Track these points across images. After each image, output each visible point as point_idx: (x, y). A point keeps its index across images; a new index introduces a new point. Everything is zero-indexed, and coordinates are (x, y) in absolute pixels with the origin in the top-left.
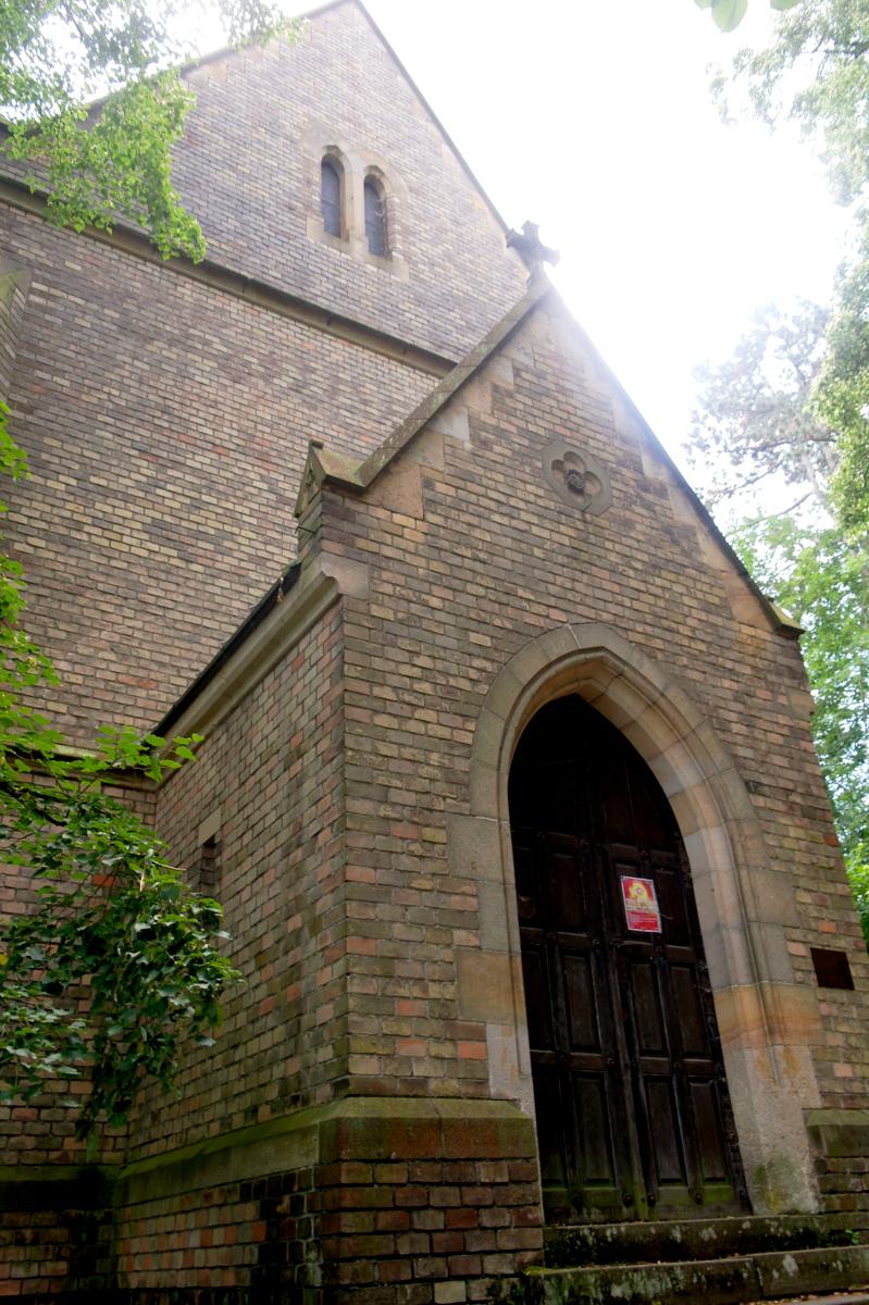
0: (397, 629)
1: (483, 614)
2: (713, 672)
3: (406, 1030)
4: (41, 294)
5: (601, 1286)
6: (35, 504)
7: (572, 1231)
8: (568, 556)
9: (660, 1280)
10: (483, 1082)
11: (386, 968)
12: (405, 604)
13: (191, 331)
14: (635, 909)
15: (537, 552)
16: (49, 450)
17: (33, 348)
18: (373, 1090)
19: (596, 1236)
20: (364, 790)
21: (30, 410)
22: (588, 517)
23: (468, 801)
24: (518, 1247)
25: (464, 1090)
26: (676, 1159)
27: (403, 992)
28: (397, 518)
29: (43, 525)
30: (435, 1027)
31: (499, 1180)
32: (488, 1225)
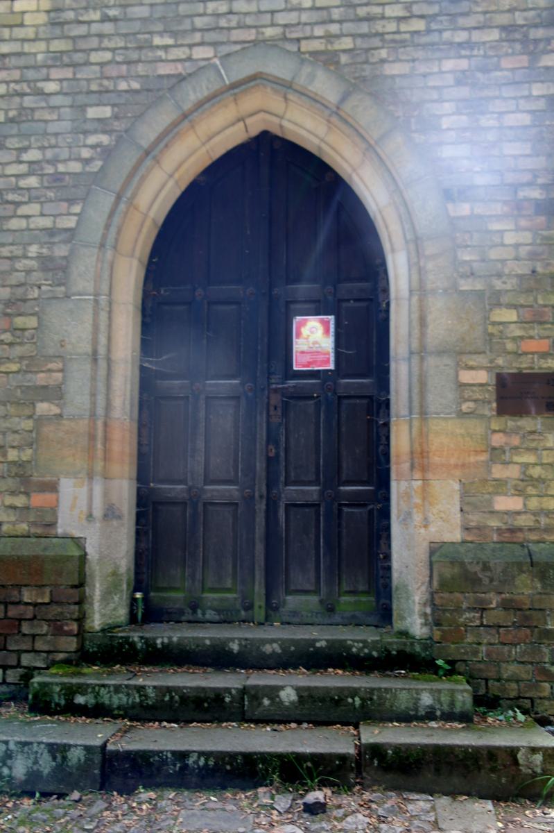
1: (106, 83)
5: (65, 695)
7: (122, 637)
9: (128, 695)
10: (53, 525)
14: (305, 348)
19: (146, 643)
23: (63, 284)
24: (52, 649)
30: (11, 483)
31: (40, 601)
32: (26, 632)
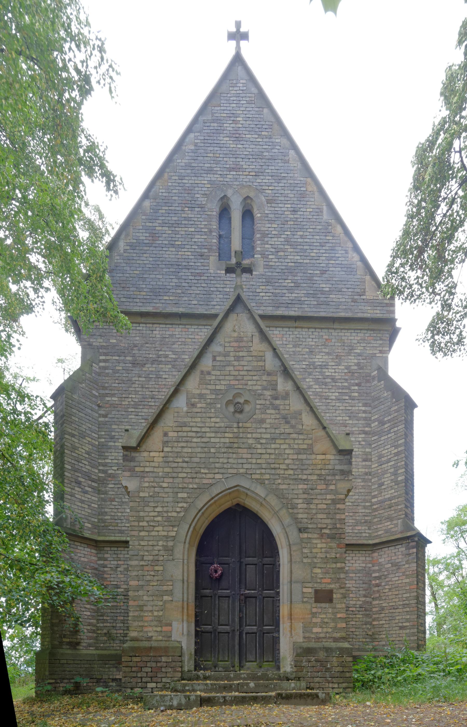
0: (149, 499)
1: (185, 485)
2: (294, 483)
3: (146, 624)
4: (105, 361)
6: (113, 454)
8: (227, 448)
11: (141, 608)
12: (153, 489)
13: (161, 353)
15: (213, 450)
16: (114, 430)
17: (104, 388)
18: (134, 639)
20: (135, 557)
21: (105, 416)
22: (241, 425)
25: (164, 639)
26: (254, 656)
27: (146, 615)
28: (152, 454)
29: (116, 461)
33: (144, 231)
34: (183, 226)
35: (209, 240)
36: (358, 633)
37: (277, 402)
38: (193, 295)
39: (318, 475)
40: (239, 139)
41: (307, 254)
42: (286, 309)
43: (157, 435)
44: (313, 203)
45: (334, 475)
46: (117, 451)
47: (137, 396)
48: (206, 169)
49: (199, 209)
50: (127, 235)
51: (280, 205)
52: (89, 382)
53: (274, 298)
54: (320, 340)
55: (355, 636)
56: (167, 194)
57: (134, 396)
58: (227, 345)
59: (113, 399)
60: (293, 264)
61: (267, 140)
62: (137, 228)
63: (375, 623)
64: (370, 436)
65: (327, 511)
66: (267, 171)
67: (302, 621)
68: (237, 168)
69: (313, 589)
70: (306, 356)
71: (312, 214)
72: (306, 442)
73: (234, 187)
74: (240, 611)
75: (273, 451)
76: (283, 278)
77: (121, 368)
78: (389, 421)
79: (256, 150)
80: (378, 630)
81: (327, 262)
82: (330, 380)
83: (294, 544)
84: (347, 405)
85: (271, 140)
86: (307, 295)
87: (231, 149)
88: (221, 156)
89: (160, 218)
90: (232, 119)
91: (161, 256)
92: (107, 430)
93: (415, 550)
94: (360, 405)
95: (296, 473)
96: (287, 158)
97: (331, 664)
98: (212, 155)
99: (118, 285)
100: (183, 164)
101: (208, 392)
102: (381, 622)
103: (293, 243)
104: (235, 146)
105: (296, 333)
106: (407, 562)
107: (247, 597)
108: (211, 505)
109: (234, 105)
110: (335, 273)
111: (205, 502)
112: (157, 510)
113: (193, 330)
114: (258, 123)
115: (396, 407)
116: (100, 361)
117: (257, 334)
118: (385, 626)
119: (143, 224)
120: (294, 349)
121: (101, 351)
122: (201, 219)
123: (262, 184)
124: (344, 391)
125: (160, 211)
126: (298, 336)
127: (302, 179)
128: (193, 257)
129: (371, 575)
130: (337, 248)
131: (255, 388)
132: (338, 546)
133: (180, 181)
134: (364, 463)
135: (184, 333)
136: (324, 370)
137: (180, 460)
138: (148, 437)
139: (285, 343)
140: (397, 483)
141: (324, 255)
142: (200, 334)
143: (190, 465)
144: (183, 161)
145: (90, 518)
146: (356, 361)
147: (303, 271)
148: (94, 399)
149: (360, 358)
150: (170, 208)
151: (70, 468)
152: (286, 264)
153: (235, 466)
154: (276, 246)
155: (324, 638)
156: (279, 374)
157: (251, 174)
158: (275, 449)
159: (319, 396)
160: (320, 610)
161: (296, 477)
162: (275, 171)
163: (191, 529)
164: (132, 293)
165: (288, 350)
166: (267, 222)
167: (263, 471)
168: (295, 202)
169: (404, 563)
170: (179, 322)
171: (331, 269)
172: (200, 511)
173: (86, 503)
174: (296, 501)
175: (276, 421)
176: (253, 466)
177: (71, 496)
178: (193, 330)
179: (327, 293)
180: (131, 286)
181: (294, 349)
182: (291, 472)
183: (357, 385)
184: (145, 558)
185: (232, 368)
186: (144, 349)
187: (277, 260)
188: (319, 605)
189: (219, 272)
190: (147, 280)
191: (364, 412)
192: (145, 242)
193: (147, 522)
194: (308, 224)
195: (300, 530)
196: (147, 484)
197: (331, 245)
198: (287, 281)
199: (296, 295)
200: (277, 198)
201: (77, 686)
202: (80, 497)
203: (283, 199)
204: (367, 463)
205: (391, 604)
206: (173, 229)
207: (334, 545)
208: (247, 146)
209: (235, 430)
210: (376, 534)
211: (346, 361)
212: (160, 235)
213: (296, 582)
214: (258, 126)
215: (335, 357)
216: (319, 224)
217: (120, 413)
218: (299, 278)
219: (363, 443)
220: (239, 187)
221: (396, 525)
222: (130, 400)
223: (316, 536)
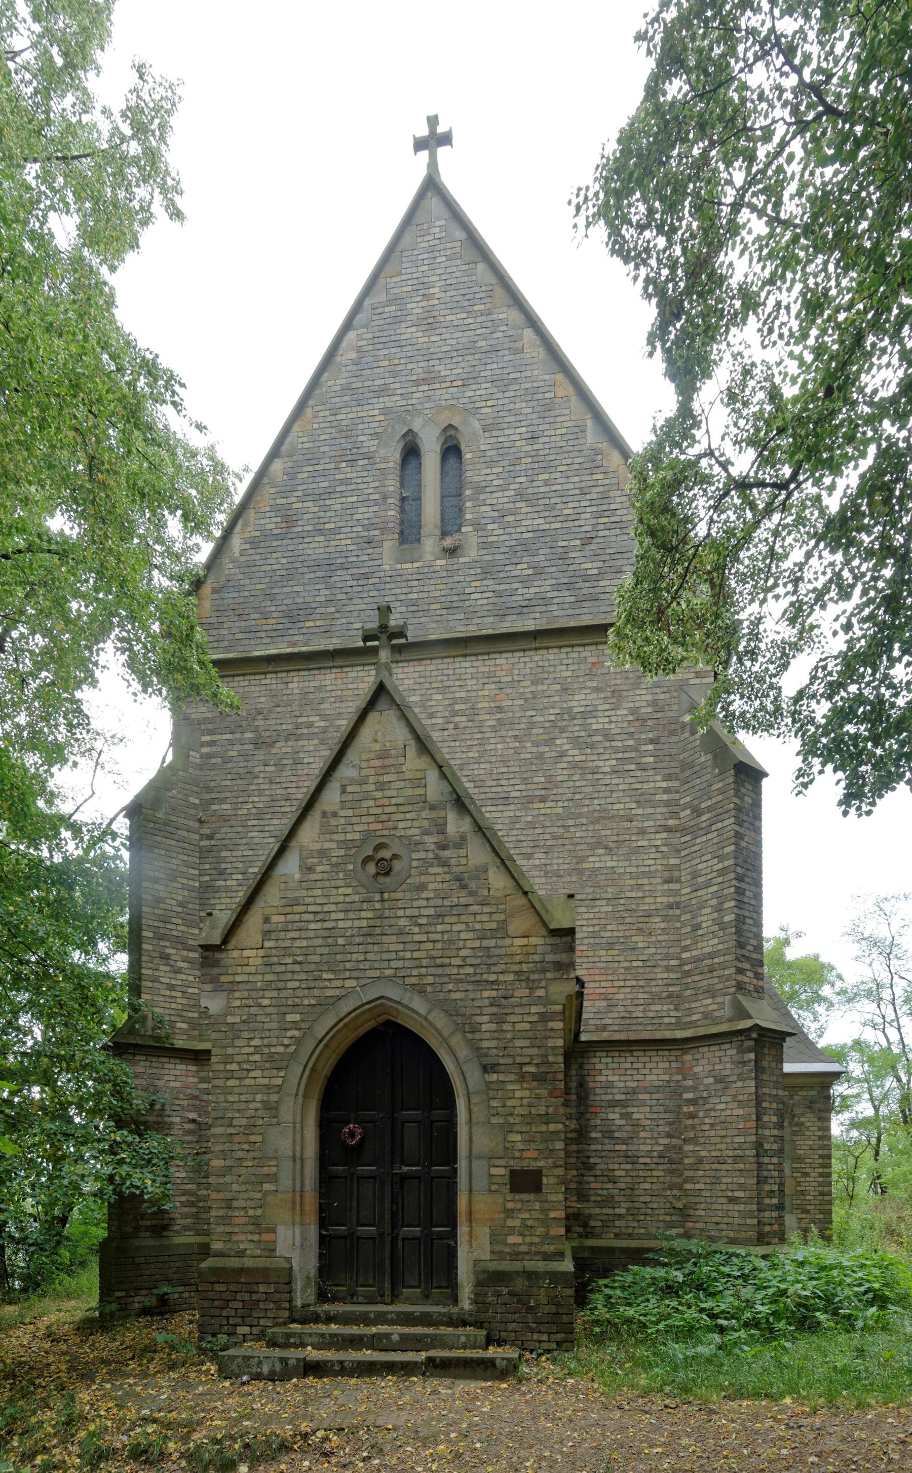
0: (241, 1027)
3: (236, 1230)
4: (210, 744)
6: (222, 900)
10: (274, 1250)
11: (229, 1204)
13: (301, 720)
15: (341, 941)
17: (209, 790)
18: (221, 1254)
20: (220, 1122)
21: (210, 837)
27: (236, 1214)
28: (246, 953)
33: (273, 514)
34: (338, 495)
35: (383, 513)
36: (655, 1206)
37: (446, 853)
38: (355, 614)
39: (516, 973)
40: (434, 326)
41: (556, 513)
42: (519, 617)
43: (254, 921)
44: (567, 418)
45: (544, 971)
46: (229, 894)
47: (262, 799)
48: (377, 388)
49: (366, 461)
50: (246, 525)
51: (507, 432)
52: (183, 785)
53: (495, 600)
54: (582, 667)
55: (649, 1211)
56: (311, 445)
57: (256, 799)
58: (364, 765)
59: (224, 806)
60: (531, 535)
61: (484, 318)
62: (262, 510)
63: (688, 1186)
64: (678, 835)
65: (531, 1034)
66: (483, 374)
67: (489, 1224)
68: (431, 378)
69: (508, 1169)
70: (556, 699)
71: (566, 437)
72: (495, 917)
73: (425, 412)
74: (393, 1201)
75: (438, 937)
76: (513, 561)
77: (235, 753)
78: (709, 809)
79: (464, 340)
80: (692, 1199)
81: (594, 521)
82: (600, 738)
83: (475, 1093)
84: (633, 780)
85: (490, 318)
86: (558, 587)
87: (419, 347)
88: (402, 361)
89: (300, 487)
90: (421, 292)
91: (301, 552)
92: (213, 860)
93: (752, 1056)
94: (658, 778)
95: (478, 971)
96: (519, 345)
97: (536, 1300)
98: (386, 363)
99: (231, 613)
100: (338, 388)
101: (334, 845)
102: (698, 1186)
103: (531, 497)
104: (426, 339)
105: (537, 658)
106: (741, 1077)
107: (404, 1178)
108: (338, 1032)
109: (426, 268)
110: (608, 539)
111: (328, 1028)
112: (253, 1043)
113: (355, 674)
114: (466, 291)
115: (720, 785)
116: (203, 745)
117: (412, 743)
118: (704, 1194)
119: (272, 502)
120: (533, 689)
121: (203, 727)
122: (368, 479)
123: (474, 399)
124: (626, 755)
125: (300, 476)
126: (540, 663)
127: (547, 377)
128: (354, 547)
129: (681, 1095)
130: (612, 494)
131: (410, 832)
132: (551, 1094)
133: (333, 418)
134: (666, 887)
135: (340, 681)
136: (589, 721)
137: (289, 960)
138: (239, 926)
139: (516, 678)
140: (723, 926)
141: (588, 509)
142: (366, 679)
143: (306, 967)
144: (339, 382)
145: (185, 1013)
146: (650, 697)
147: (549, 545)
148: (192, 812)
149: (658, 690)
150: (316, 467)
151: (151, 935)
152: (518, 536)
153: (376, 965)
154: (500, 507)
155: (526, 1253)
156: (449, 806)
157: (455, 384)
158: (442, 933)
159: (579, 768)
160: (519, 1206)
161: (478, 978)
162: (498, 372)
163: (307, 1073)
164: (253, 623)
165: (522, 690)
166: (484, 465)
167: (423, 971)
168: (534, 422)
169: (735, 1078)
170: (331, 664)
171: (601, 534)
172: (320, 1041)
173: (178, 988)
174: (479, 1019)
175: (445, 885)
176: (407, 964)
177: (153, 982)
178: (355, 674)
179: (594, 578)
180: (251, 611)
181: (533, 689)
182: (470, 970)
183: (651, 741)
184: (235, 1122)
185: (371, 803)
186: (273, 716)
187: (501, 532)
188: (518, 1196)
189: (399, 566)
190: (278, 597)
191: (666, 791)
192: (275, 532)
193: (239, 1063)
194: (558, 457)
195: (486, 1069)
196: (237, 1003)
197: (601, 489)
198: (520, 567)
199: (537, 590)
200: (501, 420)
201: (163, 1300)
202: (167, 981)
203: (512, 419)
204: (671, 886)
205: (714, 1154)
206: (321, 503)
207: (543, 1092)
208: (449, 336)
209: (378, 906)
210: (689, 1019)
211: (630, 699)
212: (300, 517)
213: (479, 1157)
214: (467, 297)
215: (609, 694)
216: (578, 454)
217: (234, 829)
218: (543, 558)
219: (665, 849)
220: (433, 411)
221: (722, 1006)
222: (251, 806)
223: (512, 1077)
